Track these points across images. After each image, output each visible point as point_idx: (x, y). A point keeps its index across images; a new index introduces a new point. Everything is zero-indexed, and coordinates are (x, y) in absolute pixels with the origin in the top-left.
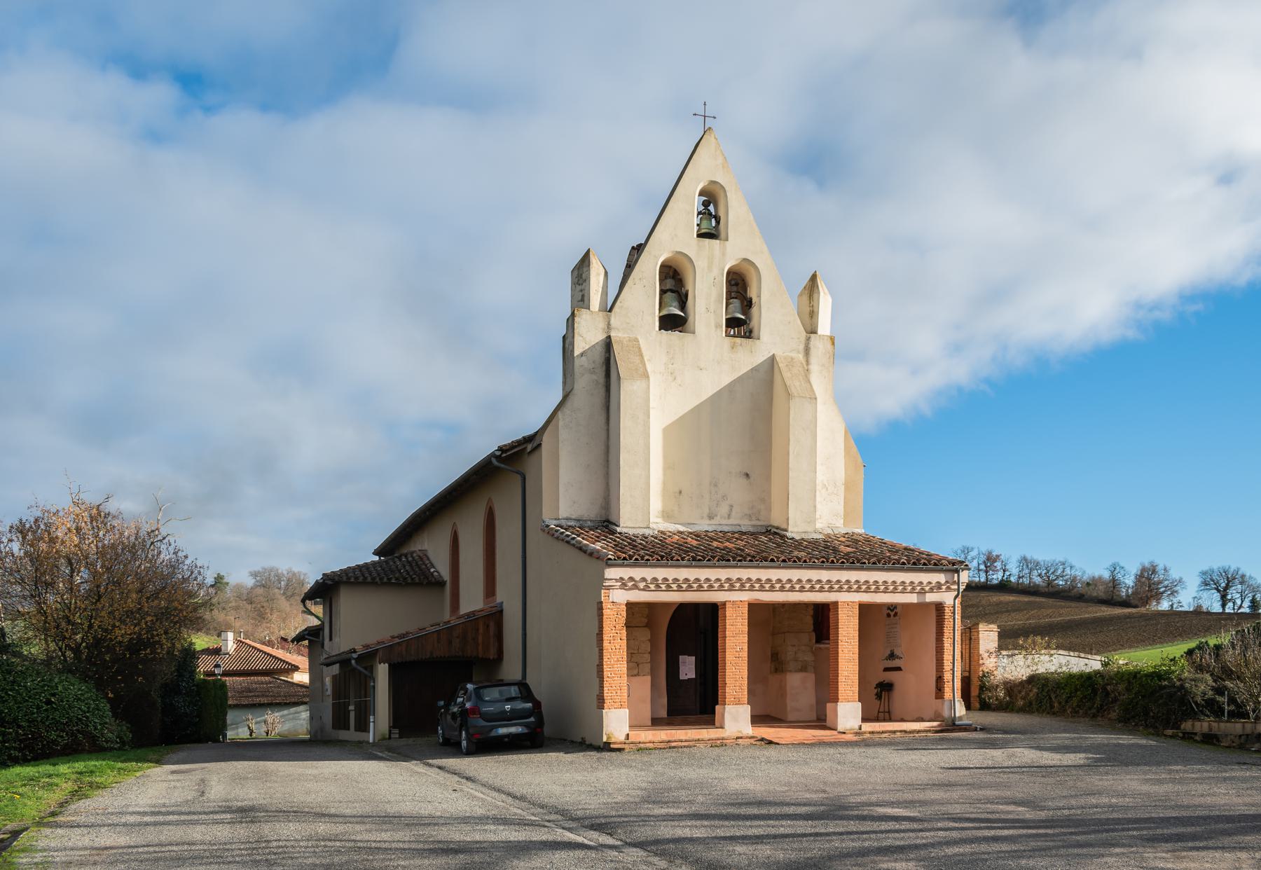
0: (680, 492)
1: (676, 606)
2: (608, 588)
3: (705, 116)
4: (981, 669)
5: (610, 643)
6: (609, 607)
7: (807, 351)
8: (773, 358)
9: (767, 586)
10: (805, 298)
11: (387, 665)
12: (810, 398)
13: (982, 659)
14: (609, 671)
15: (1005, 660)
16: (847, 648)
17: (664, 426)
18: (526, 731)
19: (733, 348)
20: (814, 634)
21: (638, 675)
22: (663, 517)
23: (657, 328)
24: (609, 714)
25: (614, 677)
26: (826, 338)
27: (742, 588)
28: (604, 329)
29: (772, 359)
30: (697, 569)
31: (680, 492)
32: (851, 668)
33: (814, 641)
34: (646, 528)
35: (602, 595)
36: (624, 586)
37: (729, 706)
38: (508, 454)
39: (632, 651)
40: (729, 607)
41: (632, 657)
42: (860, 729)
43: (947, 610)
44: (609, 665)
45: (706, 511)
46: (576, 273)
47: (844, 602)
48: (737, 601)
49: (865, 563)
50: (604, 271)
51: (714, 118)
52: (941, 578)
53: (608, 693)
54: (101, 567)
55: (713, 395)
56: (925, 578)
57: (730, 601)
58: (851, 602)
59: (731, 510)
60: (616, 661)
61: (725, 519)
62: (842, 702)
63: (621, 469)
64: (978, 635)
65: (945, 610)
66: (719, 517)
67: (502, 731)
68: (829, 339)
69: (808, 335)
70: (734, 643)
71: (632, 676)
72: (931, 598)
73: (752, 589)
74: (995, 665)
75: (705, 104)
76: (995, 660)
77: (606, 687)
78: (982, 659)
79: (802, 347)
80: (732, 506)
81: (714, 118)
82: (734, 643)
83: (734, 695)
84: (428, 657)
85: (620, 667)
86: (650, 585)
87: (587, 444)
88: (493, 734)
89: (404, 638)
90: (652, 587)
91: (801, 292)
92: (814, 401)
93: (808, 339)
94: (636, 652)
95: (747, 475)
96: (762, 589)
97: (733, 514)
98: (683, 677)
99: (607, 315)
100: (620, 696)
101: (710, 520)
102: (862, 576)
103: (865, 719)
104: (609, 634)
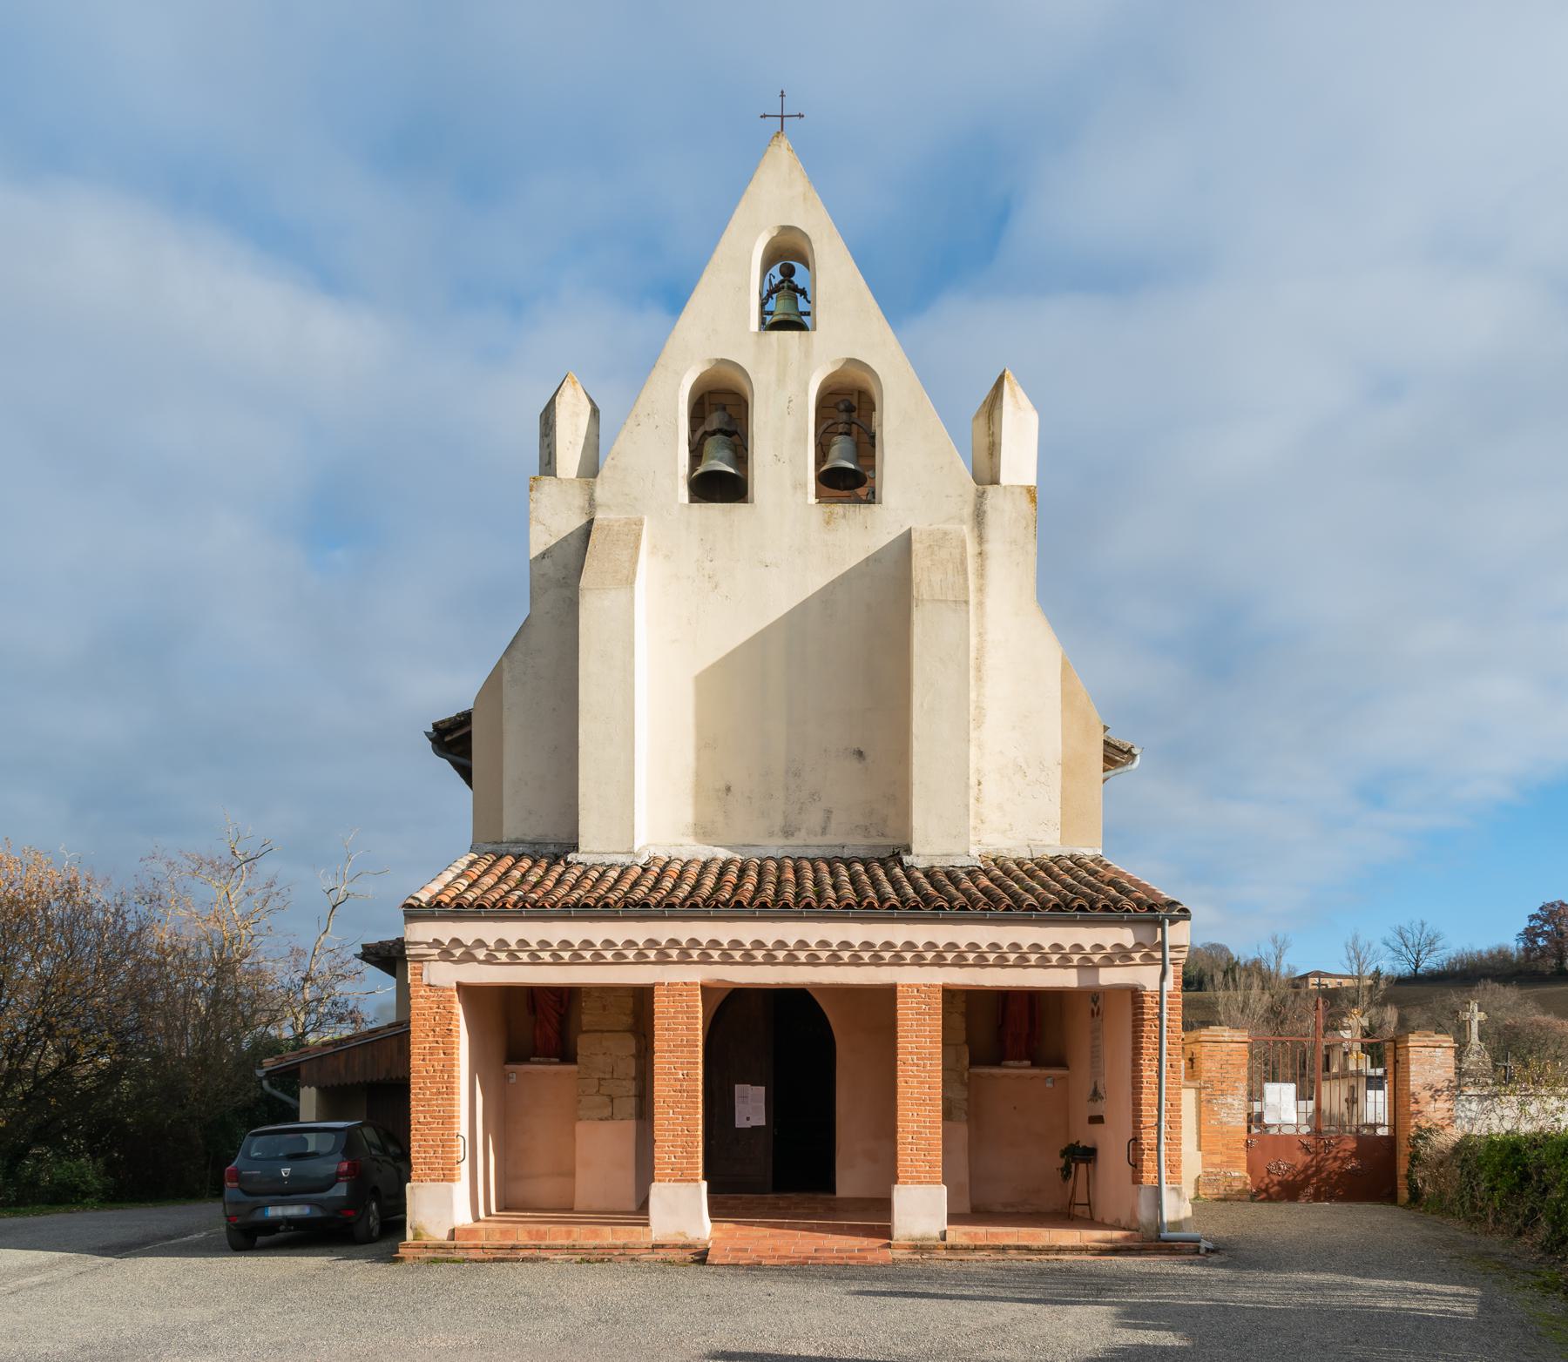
0: (728, 789)
1: (723, 996)
2: (420, 959)
3: (782, 117)
4: (1413, 1122)
5: (423, 1060)
6: (422, 993)
7: (979, 517)
8: (906, 540)
9: (866, 956)
10: (982, 421)
11: (313, 1089)
12: (956, 601)
13: (1417, 1102)
14: (421, 1112)
15: (1474, 1106)
16: (915, 1076)
17: (697, 673)
18: (318, 1214)
19: (828, 523)
20: (965, 1050)
21: (612, 1117)
22: (696, 834)
23: (686, 499)
24: (417, 1191)
25: (429, 1123)
26: (1019, 490)
27: (685, 959)
28: (583, 508)
29: (906, 540)
30: (904, 925)
31: (728, 789)
32: (926, 1116)
33: (966, 1062)
34: (627, 853)
35: (409, 971)
36: (446, 955)
37: (662, 1184)
38: (455, 735)
39: (602, 1076)
40: (660, 995)
41: (600, 1085)
42: (944, 1239)
43: (1149, 1002)
44: (421, 1100)
45: (779, 821)
46: (544, 417)
47: (909, 986)
48: (677, 984)
49: (941, 908)
50: (589, 408)
51: (800, 116)
53: (418, 1152)
54: (108, 938)
56: (1086, 936)
57: (663, 984)
58: (925, 985)
60: (436, 1094)
61: (816, 835)
62: (906, 1183)
63: (580, 750)
64: (1408, 1055)
65: (1143, 1002)
66: (803, 832)
67: (274, 1212)
68: (1025, 492)
69: (980, 487)
71: (601, 1120)
72: (1109, 977)
73: (705, 959)
74: (1448, 1115)
75: (782, 96)
76: (1447, 1105)
77: (416, 1140)
78: (1417, 1102)
79: (968, 510)
80: (829, 812)
81: (800, 116)
83: (672, 1164)
84: (381, 1078)
85: (442, 1105)
86: (497, 954)
87: (554, 709)
88: (257, 1216)
89: (342, 1045)
90: (503, 957)
91: (978, 413)
92: (963, 606)
93: (981, 496)
94: (607, 1077)
95: (860, 754)
96: (727, 960)
97: (833, 825)
98: (741, 1122)
99: (588, 484)
102: (942, 934)
103: (954, 1218)
104: (421, 1043)
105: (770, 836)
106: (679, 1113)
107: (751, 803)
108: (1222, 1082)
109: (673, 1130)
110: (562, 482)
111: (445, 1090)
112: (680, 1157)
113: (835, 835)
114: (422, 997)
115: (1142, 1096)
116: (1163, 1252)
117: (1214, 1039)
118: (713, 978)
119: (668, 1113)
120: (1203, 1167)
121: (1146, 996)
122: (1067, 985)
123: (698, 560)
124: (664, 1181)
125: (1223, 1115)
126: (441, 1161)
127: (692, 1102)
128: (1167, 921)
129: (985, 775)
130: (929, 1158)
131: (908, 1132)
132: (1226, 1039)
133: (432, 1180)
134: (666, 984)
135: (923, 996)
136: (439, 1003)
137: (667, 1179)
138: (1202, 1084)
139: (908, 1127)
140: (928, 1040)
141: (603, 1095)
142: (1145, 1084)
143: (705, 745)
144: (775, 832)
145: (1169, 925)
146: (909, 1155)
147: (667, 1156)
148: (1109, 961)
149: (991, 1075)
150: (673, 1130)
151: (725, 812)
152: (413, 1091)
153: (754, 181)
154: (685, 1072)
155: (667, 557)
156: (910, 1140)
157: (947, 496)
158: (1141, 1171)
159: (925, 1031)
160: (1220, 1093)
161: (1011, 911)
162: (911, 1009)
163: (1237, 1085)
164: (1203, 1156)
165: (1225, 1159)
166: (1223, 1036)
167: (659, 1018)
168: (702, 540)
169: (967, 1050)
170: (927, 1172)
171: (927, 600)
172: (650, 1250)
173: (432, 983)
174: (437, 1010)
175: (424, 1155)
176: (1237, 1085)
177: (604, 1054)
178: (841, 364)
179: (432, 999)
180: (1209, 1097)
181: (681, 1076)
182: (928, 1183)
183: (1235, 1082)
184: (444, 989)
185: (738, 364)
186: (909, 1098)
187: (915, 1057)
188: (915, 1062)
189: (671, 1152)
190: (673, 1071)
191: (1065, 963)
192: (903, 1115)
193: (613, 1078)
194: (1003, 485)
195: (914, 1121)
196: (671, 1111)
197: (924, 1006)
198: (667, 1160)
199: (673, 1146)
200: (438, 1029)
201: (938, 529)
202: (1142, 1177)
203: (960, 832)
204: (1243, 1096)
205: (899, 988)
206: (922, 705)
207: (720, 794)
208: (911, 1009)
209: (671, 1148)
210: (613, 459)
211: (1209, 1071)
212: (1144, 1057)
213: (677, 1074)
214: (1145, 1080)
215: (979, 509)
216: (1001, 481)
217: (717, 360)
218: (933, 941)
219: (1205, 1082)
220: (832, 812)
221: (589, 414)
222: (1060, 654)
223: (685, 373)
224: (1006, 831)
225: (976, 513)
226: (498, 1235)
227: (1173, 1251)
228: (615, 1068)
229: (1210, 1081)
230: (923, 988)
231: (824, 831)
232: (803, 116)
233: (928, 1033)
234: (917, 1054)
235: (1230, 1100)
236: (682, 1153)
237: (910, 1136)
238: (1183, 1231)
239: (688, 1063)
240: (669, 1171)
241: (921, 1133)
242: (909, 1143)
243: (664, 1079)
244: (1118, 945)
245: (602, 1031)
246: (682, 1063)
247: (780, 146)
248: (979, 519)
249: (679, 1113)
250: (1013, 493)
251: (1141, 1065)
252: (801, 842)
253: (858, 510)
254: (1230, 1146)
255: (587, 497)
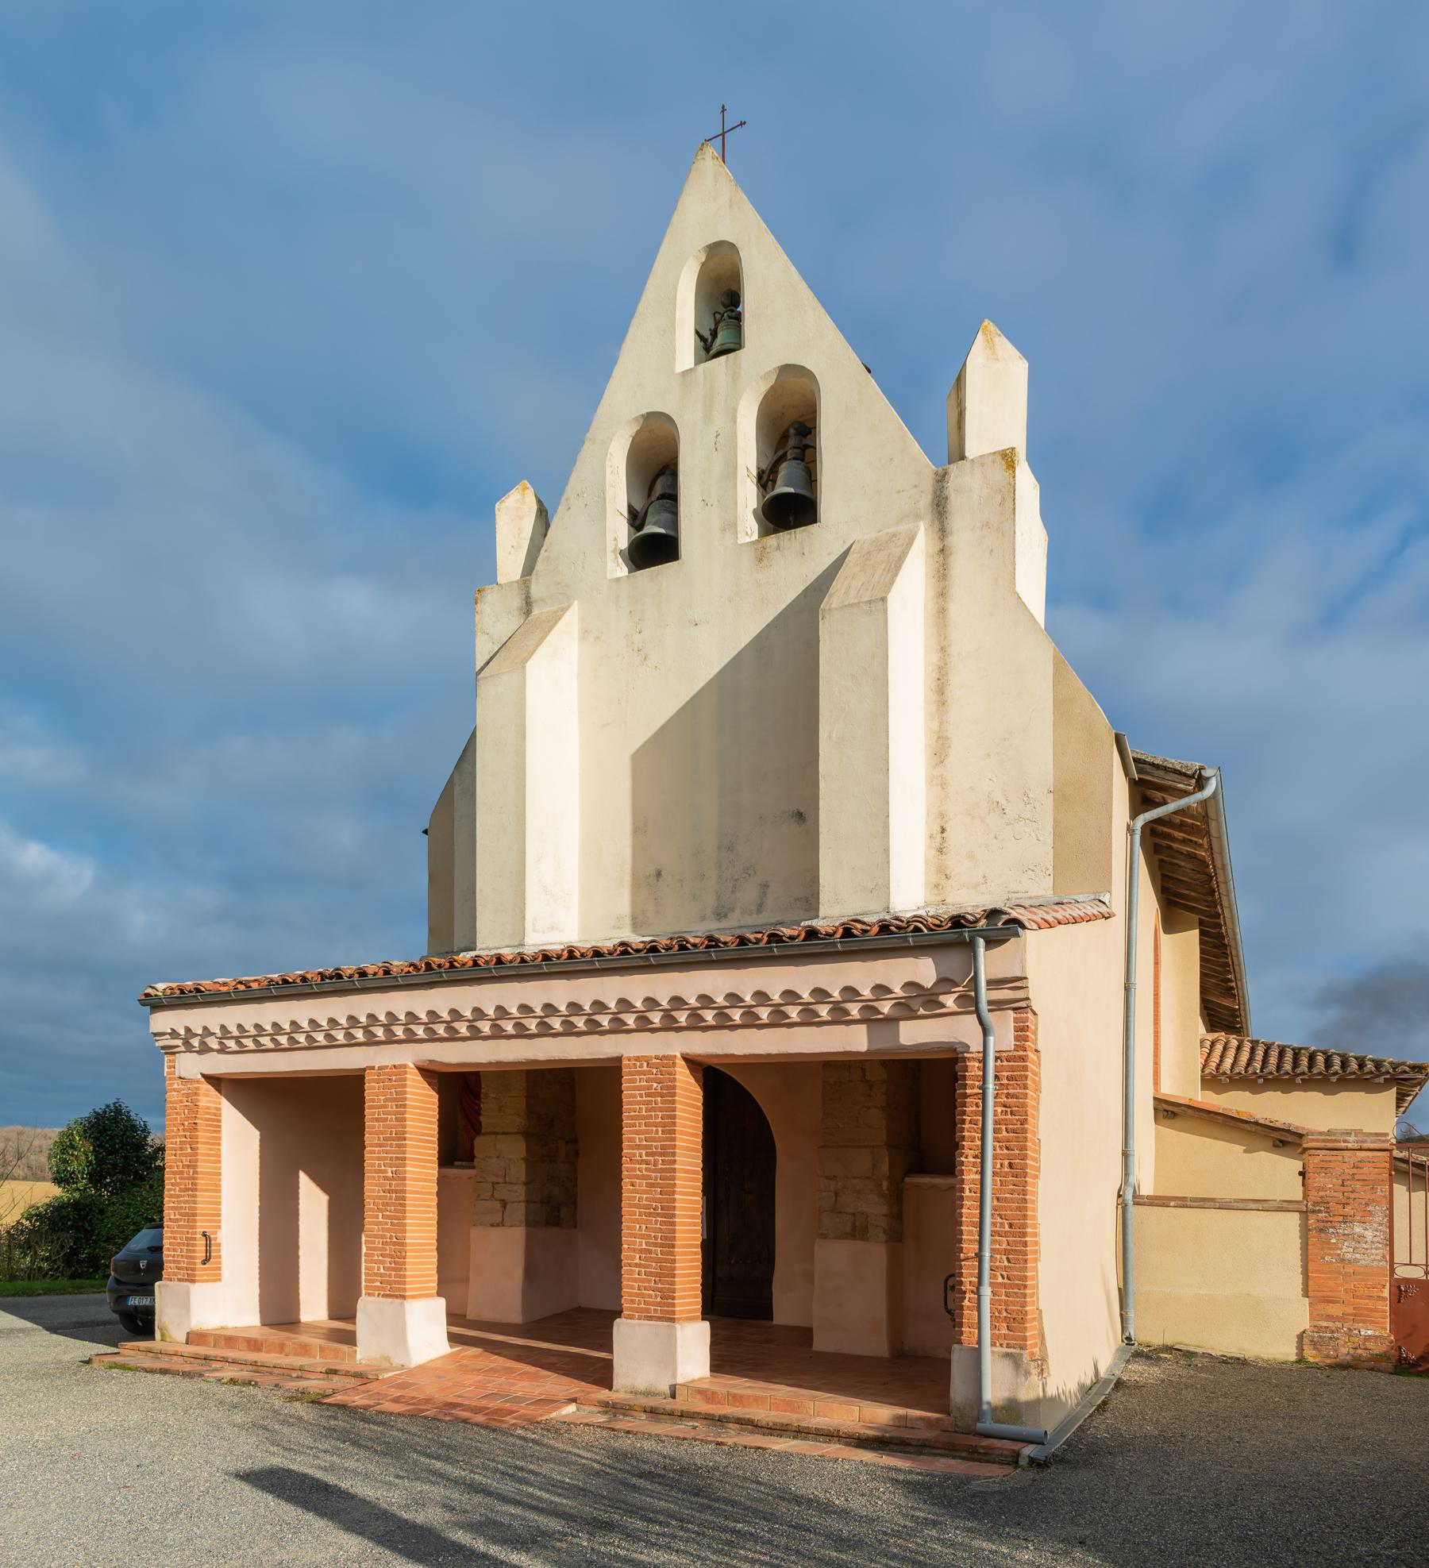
0: (659, 874)
6: (176, 1086)
21: (501, 1224)
26: (991, 458)
31: (659, 874)
39: (495, 1179)
45: (711, 903)
47: (637, 1059)
51: (723, 110)
52: (924, 970)
55: (724, 668)
58: (657, 1058)
59: (765, 893)
62: (631, 1317)
65: (966, 1069)
66: (737, 911)
68: (998, 458)
70: (379, 1159)
71: (492, 1225)
72: (915, 1034)
79: (925, 501)
80: (765, 886)
81: (723, 110)
82: (379, 1159)
83: (381, 1275)
92: (880, 605)
94: (500, 1180)
100: (187, 1257)
101: (719, 920)
105: (702, 921)
106: (388, 1217)
107: (682, 886)
108: (1344, 1205)
109: (383, 1237)
110: (502, 588)
111: (190, 1186)
112: (389, 1269)
113: (772, 911)
114: (174, 1090)
115: (963, 1211)
116: (958, 1454)
117: (1330, 1145)
118: (425, 1058)
119: (377, 1217)
120: (1312, 1318)
121: (968, 1059)
122: (849, 1049)
123: (627, 635)
124: (373, 1295)
125: (1347, 1250)
126: (186, 1260)
127: (400, 1205)
128: (981, 942)
129: (950, 819)
130: (660, 1286)
131: (634, 1250)
132: (1350, 1145)
133: (179, 1280)
134: (376, 1067)
135: (655, 1071)
136: (187, 1095)
137: (377, 1293)
138: (1310, 1206)
139: (635, 1243)
140: (660, 1129)
141: (496, 1200)
142: (967, 1193)
143: (639, 829)
144: (707, 916)
145: (987, 949)
146: (636, 1280)
147: (376, 1266)
148: (906, 1010)
149: (935, 1186)
150: (383, 1237)
151: (655, 899)
152: (167, 1187)
153: (679, 208)
154: (394, 1169)
155: (597, 638)
156: (637, 1261)
157: (899, 492)
158: (961, 1325)
159: (656, 1117)
160: (1341, 1219)
161: (748, 945)
162: (639, 1088)
163: (1370, 1208)
164: (1311, 1304)
165: (1350, 1310)
166: (1345, 1141)
167: (371, 1107)
168: (631, 612)
169: (887, 1153)
170: (658, 1304)
171: (836, 609)
172: (326, 1375)
173: (182, 1076)
174: (187, 1104)
175: (173, 1253)
176: (1370, 1208)
177: (498, 1157)
178: (775, 377)
179: (182, 1092)
180: (1321, 1225)
181: (390, 1174)
182: (659, 1319)
183: (1367, 1205)
184: (190, 1081)
185: (665, 414)
186: (636, 1206)
187: (644, 1152)
188: (644, 1158)
189: (380, 1262)
190: (383, 1167)
191: (840, 1016)
192: (628, 1228)
193: (505, 1183)
194: (971, 458)
195: (642, 1237)
196: (380, 1214)
197: (655, 1085)
198: (376, 1271)
199: (382, 1255)
200: (186, 1123)
201: (887, 534)
202: (961, 1333)
203: (877, 885)
204: (1380, 1224)
205: (625, 1062)
206: (830, 737)
207: (650, 880)
208: (639, 1088)
209: (380, 1258)
210: (546, 551)
211: (1324, 1189)
212: (967, 1151)
213: (385, 1171)
214: (967, 1187)
215: (939, 497)
216: (967, 454)
217: (643, 416)
218: (652, 996)
219: (1315, 1204)
220: (768, 886)
221: (535, 511)
222: (1051, 652)
223: (611, 440)
224: (977, 885)
225: (935, 502)
226: (223, 1342)
227: (976, 1456)
228: (507, 1171)
229: (1322, 1202)
230: (654, 1061)
231: (760, 908)
232: (745, 123)
233: (659, 1120)
234: (646, 1147)
235: (1358, 1229)
236: (391, 1264)
237: (638, 1256)
238: (1022, 1423)
239: (397, 1158)
240: (379, 1284)
241: (650, 1252)
242: (637, 1265)
243: (374, 1177)
244: (909, 985)
245: (497, 1134)
246: (391, 1159)
247: (704, 159)
248: (940, 508)
249: (388, 1217)
250: (982, 465)
251: (962, 1163)
252: (735, 924)
253: (793, 536)
254: (1358, 1294)
255: (524, 596)
